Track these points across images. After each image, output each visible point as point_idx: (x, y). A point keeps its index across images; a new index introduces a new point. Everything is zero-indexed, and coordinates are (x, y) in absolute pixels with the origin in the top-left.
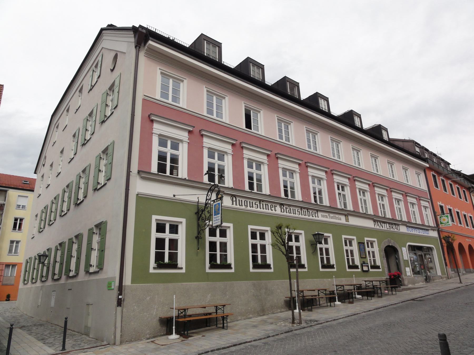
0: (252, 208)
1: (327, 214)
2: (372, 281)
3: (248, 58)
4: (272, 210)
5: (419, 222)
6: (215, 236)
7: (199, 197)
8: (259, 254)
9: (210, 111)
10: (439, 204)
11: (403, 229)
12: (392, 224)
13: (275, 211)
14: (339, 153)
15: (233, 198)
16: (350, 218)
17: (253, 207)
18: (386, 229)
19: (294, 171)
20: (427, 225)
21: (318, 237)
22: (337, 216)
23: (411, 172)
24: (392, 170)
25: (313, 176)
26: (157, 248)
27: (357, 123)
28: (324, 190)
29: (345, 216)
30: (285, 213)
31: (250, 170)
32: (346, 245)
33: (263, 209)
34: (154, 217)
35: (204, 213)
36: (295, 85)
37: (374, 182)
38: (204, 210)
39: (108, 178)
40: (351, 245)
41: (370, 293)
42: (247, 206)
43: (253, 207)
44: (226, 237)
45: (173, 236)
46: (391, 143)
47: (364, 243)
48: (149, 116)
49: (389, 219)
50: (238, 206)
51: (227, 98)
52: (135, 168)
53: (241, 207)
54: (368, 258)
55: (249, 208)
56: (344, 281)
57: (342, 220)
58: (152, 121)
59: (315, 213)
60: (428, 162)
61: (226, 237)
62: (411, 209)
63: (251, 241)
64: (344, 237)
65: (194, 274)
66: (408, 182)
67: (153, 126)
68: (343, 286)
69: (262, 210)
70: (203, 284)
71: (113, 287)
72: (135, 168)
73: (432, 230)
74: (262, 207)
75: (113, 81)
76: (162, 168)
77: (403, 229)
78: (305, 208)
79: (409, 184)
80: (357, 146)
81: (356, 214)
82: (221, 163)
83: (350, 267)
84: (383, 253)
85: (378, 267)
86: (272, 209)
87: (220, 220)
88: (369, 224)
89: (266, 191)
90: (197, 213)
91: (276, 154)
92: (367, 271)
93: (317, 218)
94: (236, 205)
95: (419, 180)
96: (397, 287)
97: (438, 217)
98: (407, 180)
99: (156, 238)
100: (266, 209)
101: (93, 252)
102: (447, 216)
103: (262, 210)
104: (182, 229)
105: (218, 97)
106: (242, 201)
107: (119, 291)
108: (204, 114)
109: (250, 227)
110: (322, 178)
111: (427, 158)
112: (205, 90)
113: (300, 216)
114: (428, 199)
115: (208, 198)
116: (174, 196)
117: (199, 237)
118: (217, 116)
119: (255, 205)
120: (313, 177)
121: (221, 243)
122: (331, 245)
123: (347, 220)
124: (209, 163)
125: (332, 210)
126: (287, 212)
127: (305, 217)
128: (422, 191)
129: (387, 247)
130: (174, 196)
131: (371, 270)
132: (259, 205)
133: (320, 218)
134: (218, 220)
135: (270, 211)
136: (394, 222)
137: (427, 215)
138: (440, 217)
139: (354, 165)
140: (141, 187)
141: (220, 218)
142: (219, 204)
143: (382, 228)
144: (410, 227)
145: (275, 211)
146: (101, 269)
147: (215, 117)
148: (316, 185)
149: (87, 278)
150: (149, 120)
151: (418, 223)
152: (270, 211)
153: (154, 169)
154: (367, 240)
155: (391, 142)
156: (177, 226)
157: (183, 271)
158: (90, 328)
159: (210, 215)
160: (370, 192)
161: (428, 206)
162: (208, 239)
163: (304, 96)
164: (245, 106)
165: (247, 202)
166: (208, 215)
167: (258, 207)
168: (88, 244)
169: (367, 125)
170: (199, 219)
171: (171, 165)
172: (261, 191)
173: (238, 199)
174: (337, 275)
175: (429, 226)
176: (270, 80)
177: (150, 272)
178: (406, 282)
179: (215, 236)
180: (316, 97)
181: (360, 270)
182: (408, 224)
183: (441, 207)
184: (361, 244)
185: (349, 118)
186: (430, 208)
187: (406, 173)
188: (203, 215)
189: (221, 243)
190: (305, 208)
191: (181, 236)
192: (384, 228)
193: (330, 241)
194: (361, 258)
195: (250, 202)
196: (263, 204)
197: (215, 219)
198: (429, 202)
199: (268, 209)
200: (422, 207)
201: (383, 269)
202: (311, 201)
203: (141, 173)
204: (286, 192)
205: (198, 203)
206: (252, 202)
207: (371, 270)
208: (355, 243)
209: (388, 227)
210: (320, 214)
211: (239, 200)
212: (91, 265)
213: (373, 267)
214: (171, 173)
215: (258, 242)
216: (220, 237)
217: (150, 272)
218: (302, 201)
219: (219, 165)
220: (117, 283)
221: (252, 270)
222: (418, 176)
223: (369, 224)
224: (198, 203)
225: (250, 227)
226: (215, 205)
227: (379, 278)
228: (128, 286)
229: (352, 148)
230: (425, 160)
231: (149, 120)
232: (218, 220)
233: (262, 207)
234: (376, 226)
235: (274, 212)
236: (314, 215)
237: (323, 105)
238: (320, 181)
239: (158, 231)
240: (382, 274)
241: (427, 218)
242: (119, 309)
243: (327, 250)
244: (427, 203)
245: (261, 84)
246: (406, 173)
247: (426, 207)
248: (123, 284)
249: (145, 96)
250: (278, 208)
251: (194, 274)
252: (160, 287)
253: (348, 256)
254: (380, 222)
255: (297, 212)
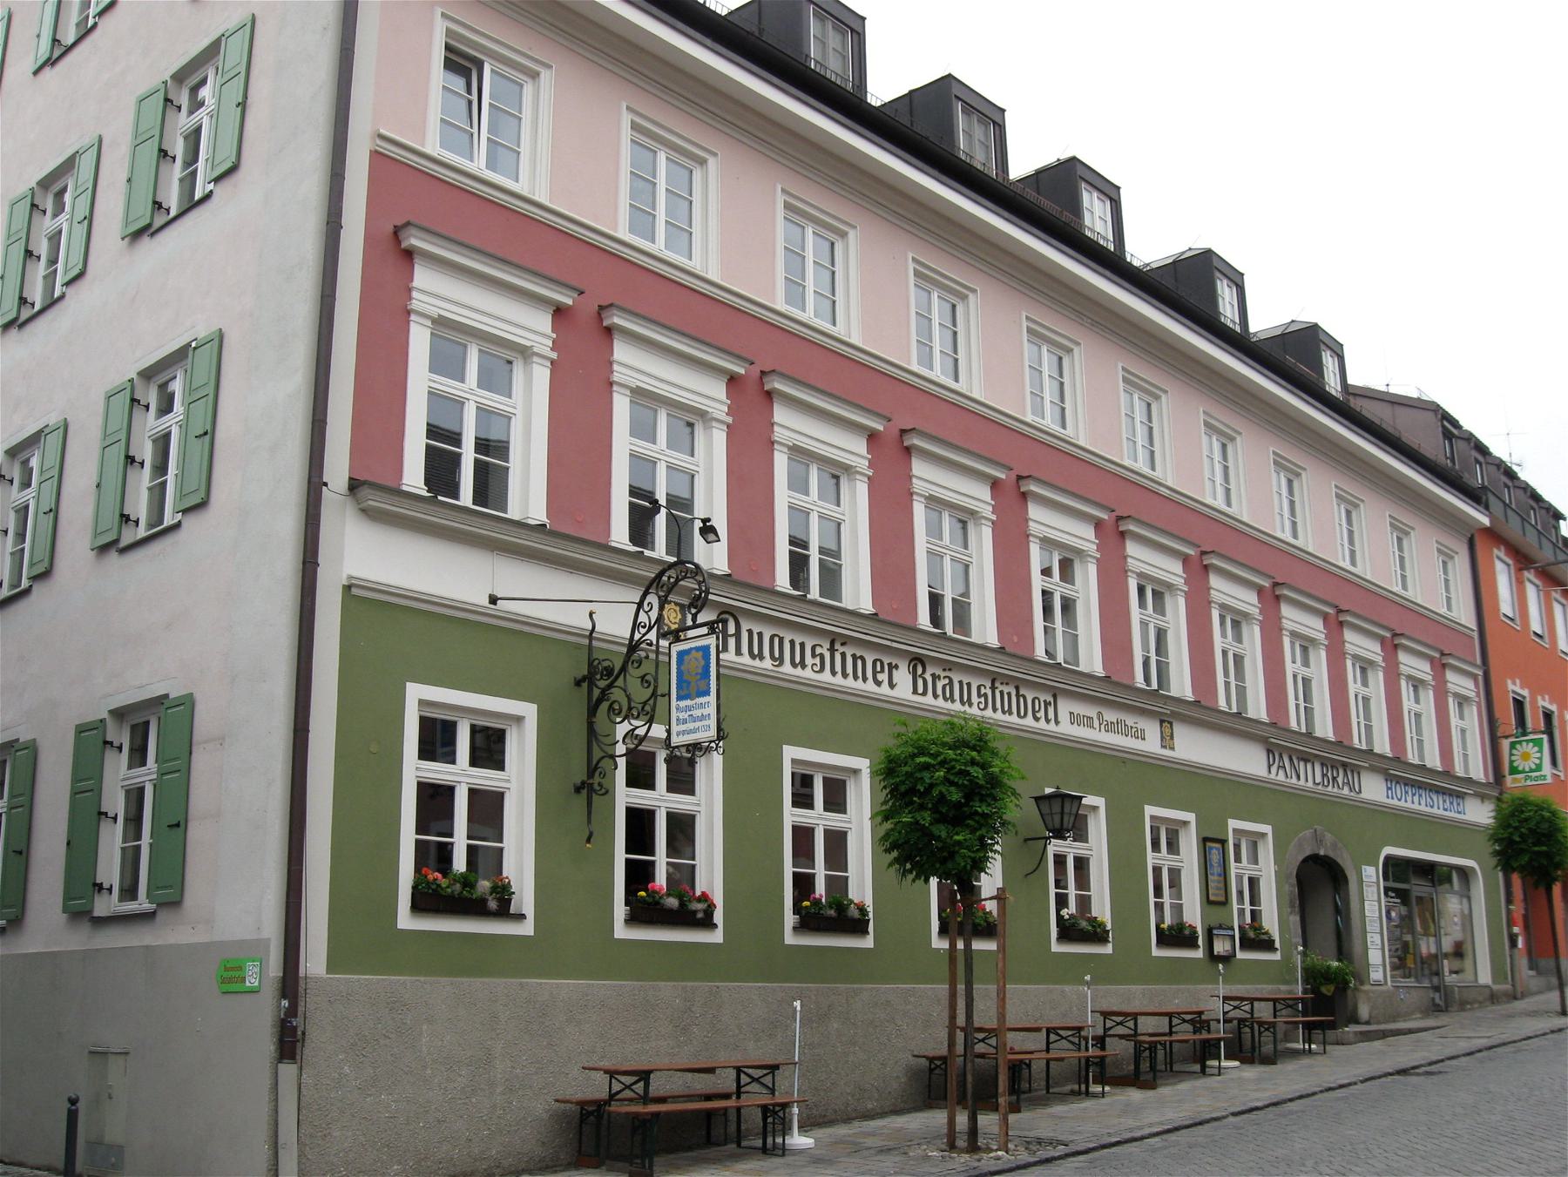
0: (799, 671)
1: (1091, 711)
2: (1252, 1000)
3: (949, 79)
4: (878, 683)
5: (1434, 761)
6: (649, 784)
7: (613, 616)
8: (820, 871)
9: (643, 217)
10: (1511, 687)
11: (1373, 789)
12: (1334, 765)
13: (892, 685)
14: (1062, 399)
15: (915, 668)
16: (1182, 733)
17: (803, 666)
18: (1310, 784)
19: (973, 513)
20: (1416, 762)
21: (1056, 808)
22: (1130, 720)
23: (1424, 542)
24: (1292, 503)
25: (638, 393)
26: (420, 829)
27: (1227, 311)
28: (854, 532)
29: (1269, 751)
30: (929, 699)
31: (643, 447)
32: (1156, 846)
33: (845, 675)
34: (416, 692)
35: (620, 682)
36: (992, 118)
37: (1283, 576)
38: (623, 669)
39: (196, 500)
40: (1173, 847)
41: (1249, 1043)
42: (781, 660)
43: (803, 666)
44: (692, 792)
45: (486, 778)
46: (1351, 408)
47: (1223, 842)
48: (396, 231)
49: (1432, 771)
50: (746, 659)
51: (546, 76)
52: (337, 470)
53: (757, 663)
54: (1235, 907)
55: (787, 668)
56: (1134, 996)
57: (1150, 742)
58: (409, 255)
59: (1047, 704)
60: (1487, 507)
61: (692, 792)
62: (1354, 687)
63: (791, 816)
64: (1150, 810)
65: (567, 946)
66: (1353, 563)
67: (1124, 548)
68: (1135, 1016)
69: (838, 680)
70: (601, 987)
71: (252, 981)
72: (337, 470)
73: (1476, 795)
74: (838, 667)
75: (206, 42)
76: (441, 470)
77: (1373, 789)
78: (1007, 680)
79: (1409, 594)
80: (1227, 418)
81: (1201, 713)
82: (494, 400)
83: (810, 921)
84: (1291, 887)
85: (1268, 945)
86: (880, 677)
87: (713, 723)
88: (1247, 761)
89: (857, 596)
90: (587, 680)
91: (903, 432)
92: (1227, 959)
93: (1052, 727)
94: (738, 652)
95: (1402, 559)
96: (1332, 1026)
97: (1505, 744)
98: (1353, 553)
99: (420, 784)
100: (856, 677)
101: (105, 827)
102: (1538, 743)
103: (838, 680)
104: (522, 751)
105: (675, 156)
106: (760, 635)
107: (284, 996)
108: (428, 150)
109: (790, 753)
110: (847, 469)
111: (1484, 488)
112: (626, 119)
113: (826, 677)
114: (1474, 665)
115: (643, 618)
116: (493, 600)
117: (592, 787)
118: (492, 164)
119: (814, 655)
120: (799, 454)
121: (672, 818)
122: (1097, 844)
123: (1167, 740)
124: (433, 395)
125: (1112, 691)
126: (935, 696)
127: (1007, 718)
128: (1448, 627)
129: (1305, 860)
130: (493, 600)
131: (1240, 955)
132: (989, 693)
133: (1066, 728)
134: (702, 718)
135: (870, 686)
136: (1342, 759)
137: (1463, 731)
138: (1513, 746)
139: (1127, 463)
140: (365, 554)
141: (712, 710)
142: (706, 649)
143: (1294, 780)
144: (1399, 780)
145: (892, 685)
146: (175, 903)
147: (659, 247)
148: (813, 499)
149: (78, 940)
150: (395, 255)
151: (1429, 765)
152: (870, 686)
153: (414, 477)
154: (1153, 818)
155: (1356, 404)
156: (500, 736)
157: (527, 928)
158: (119, 1150)
159: (654, 694)
160: (1188, 597)
161: (1472, 695)
162: (625, 796)
163: (882, 89)
164: (449, 32)
165: (781, 640)
166: (640, 694)
167: (822, 669)
168: (75, 793)
169: (1263, 320)
170: (592, 710)
171: (476, 460)
172: (967, 633)
173: (745, 626)
174: (1104, 972)
175: (1469, 781)
176: (885, 84)
177: (721, 940)
178: (1364, 1011)
179: (649, 784)
180: (1067, 177)
181: (1199, 954)
182: (1396, 770)
183: (1519, 704)
184: (1210, 842)
185: (1192, 285)
186: (1479, 704)
187: (1401, 549)
188: (616, 694)
189: (672, 818)
190: (1007, 680)
191: (519, 779)
192: (1302, 782)
193: (1098, 828)
194: (1209, 902)
195: (792, 642)
196: (843, 655)
197: (683, 715)
198: (1474, 677)
199: (865, 679)
200: (1403, 683)
201: (1287, 957)
202: (1133, 676)
203: (365, 492)
204: (798, 564)
205: (590, 637)
206: (802, 645)
207: (1240, 955)
208: (1189, 844)
209: (1318, 779)
210: (1065, 707)
211: (750, 632)
212: (100, 887)
213: (1248, 943)
214: (481, 495)
215: (819, 818)
216: (825, 810)
217: (721, 940)
218: (874, 617)
219: (482, 411)
220: (275, 968)
221: (621, 931)
222: (1399, 540)
223: (1247, 761)
224: (590, 637)
225: (790, 753)
226: (681, 654)
227: (1266, 989)
228: (318, 979)
229: (1206, 424)
230: (1474, 496)
231: (395, 255)
232: (702, 718)
233: (838, 667)
234: (1274, 770)
235: (884, 689)
236: (1041, 714)
237: (1095, 218)
238: (964, 523)
239: (426, 752)
240: (1274, 974)
241: (1464, 747)
242: (288, 1070)
243: (1082, 864)
244: (1470, 684)
245: (847, 103)
246: (1401, 549)
247: (1462, 701)
248: (302, 973)
249: (382, 137)
250: (903, 676)
251: (567, 946)
252: (439, 990)
253: (1158, 892)
254: (1292, 753)
255: (809, 660)
